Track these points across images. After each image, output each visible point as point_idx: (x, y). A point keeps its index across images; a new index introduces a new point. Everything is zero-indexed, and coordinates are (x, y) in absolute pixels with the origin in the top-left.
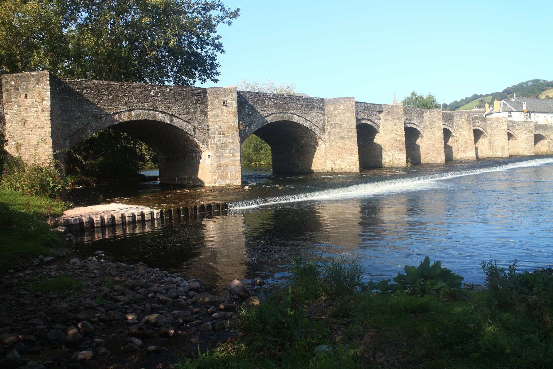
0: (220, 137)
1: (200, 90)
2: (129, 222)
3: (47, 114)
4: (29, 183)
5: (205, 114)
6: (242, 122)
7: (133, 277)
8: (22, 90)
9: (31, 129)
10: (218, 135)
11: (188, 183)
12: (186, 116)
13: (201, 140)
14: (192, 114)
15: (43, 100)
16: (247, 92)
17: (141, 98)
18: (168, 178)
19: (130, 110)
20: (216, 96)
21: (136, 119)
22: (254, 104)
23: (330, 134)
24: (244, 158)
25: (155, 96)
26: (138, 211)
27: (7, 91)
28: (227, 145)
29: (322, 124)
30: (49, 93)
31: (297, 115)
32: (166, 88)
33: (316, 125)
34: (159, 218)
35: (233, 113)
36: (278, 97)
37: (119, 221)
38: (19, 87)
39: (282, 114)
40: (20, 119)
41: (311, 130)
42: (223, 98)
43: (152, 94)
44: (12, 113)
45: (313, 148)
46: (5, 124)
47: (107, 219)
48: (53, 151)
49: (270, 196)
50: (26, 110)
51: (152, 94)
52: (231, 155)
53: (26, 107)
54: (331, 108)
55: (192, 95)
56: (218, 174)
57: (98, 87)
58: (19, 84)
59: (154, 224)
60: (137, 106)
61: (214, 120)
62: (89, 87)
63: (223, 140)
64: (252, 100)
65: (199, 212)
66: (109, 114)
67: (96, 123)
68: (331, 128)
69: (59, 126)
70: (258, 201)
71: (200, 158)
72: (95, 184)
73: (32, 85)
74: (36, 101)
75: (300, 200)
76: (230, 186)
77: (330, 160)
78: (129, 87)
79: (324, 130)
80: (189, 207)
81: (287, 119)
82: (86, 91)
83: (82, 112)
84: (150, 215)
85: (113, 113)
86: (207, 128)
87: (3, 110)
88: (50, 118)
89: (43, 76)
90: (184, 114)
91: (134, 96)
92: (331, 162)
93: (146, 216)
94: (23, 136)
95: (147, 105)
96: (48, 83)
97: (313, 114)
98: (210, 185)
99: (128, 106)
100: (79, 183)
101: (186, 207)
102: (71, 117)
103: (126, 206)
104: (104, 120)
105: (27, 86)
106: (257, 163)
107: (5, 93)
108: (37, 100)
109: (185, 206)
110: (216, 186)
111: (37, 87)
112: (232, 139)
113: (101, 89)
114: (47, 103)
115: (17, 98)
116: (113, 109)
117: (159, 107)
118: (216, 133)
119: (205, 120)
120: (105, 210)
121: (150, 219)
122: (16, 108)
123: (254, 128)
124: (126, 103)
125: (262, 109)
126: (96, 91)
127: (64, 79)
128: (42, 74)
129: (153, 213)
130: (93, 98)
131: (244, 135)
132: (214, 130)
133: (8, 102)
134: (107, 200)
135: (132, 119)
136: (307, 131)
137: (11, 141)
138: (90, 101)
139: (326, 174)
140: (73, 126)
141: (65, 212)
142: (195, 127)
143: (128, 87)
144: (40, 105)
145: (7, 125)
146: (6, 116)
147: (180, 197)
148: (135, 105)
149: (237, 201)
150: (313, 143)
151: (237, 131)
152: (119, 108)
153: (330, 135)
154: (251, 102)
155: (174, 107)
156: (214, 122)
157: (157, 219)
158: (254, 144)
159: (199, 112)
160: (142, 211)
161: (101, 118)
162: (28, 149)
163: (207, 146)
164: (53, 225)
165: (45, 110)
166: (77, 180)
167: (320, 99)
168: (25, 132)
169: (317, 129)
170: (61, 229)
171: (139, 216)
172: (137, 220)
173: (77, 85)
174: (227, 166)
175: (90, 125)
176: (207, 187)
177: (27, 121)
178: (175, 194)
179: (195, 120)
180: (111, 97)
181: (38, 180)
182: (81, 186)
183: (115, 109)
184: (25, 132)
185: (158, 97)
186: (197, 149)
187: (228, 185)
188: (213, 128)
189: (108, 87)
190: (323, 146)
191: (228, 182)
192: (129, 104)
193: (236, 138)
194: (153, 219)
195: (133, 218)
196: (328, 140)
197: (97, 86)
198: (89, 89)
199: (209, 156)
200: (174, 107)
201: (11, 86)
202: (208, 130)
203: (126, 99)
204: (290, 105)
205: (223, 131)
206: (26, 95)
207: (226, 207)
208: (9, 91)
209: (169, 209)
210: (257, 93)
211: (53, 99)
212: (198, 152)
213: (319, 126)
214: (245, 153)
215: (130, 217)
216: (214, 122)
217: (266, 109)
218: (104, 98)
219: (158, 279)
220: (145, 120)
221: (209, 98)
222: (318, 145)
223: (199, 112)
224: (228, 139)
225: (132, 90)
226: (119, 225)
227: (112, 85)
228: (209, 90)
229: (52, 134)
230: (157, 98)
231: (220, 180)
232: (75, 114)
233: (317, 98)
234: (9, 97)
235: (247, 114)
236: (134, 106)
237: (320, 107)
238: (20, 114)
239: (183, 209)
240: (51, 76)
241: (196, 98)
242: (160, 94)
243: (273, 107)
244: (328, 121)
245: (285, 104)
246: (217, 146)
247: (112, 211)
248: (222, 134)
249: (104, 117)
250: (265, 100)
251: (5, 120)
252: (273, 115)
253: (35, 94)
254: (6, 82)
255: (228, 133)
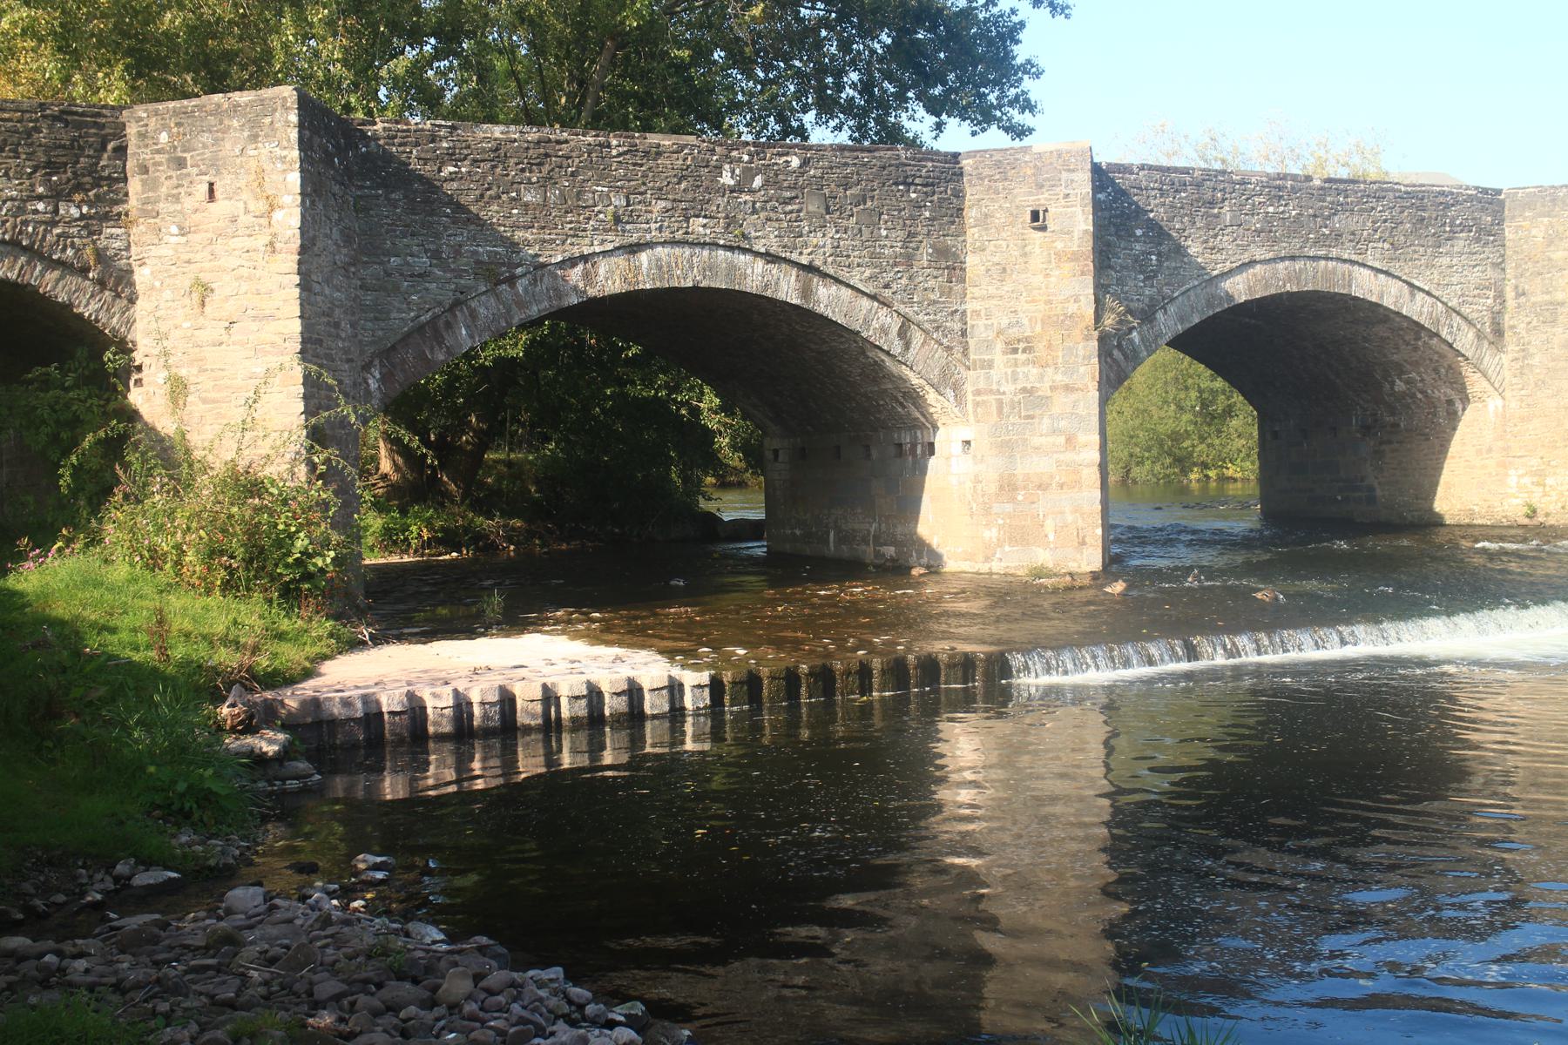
0: (1016, 365)
1: (933, 161)
2: (574, 720)
3: (288, 261)
4: (201, 538)
5: (950, 264)
6: (1116, 296)
7: (402, 1015)
8: (198, 166)
9: (227, 324)
10: (1004, 353)
11: (878, 554)
12: (867, 273)
13: (935, 375)
14: (895, 264)
15: (272, 208)
16: (1142, 167)
17: (677, 197)
18: (798, 532)
19: (633, 249)
20: (1000, 185)
21: (658, 285)
22: (1171, 220)
23: (1525, 352)
24: (1155, 452)
25: (737, 189)
26: (617, 676)
27: (144, 170)
28: (1042, 398)
29: (1490, 309)
30: (295, 178)
31: (1372, 268)
32: (787, 154)
33: (1458, 313)
34: (705, 708)
35: (1074, 257)
36: (1279, 187)
37: (534, 716)
38: (187, 155)
39: (1299, 265)
40: (187, 283)
41: (1437, 335)
42: (1031, 194)
43: (727, 179)
44: (160, 257)
45: (1442, 412)
46: (132, 301)
47: (482, 703)
48: (309, 412)
49: (1211, 630)
50: (209, 248)
51: (727, 179)
52: (1062, 440)
53: (209, 235)
54: (1534, 232)
55: (897, 184)
56: (1001, 522)
57: (502, 152)
58: (188, 141)
59: (683, 733)
60: (660, 229)
61: (992, 290)
62: (466, 152)
63: (1026, 376)
64: (1163, 204)
65: (881, 690)
66: (544, 266)
67: (492, 300)
68: (1534, 323)
69: (337, 311)
70: (1153, 650)
71: (930, 450)
72: (512, 547)
73: (235, 143)
74: (247, 211)
75: (1350, 652)
76: (1049, 576)
77: (1521, 472)
78: (632, 150)
79: (1498, 332)
80: (838, 666)
81: (1322, 286)
82: (452, 169)
83: (436, 254)
84: (664, 692)
85: (560, 258)
86: (957, 326)
87: (128, 248)
88: (297, 279)
89: (275, 110)
90: (858, 265)
91: (652, 189)
92: (1527, 480)
93: (647, 696)
94: (197, 350)
95: (704, 226)
96: (294, 134)
97: (1445, 261)
98: (966, 566)
99: (624, 231)
100: (449, 539)
101: (824, 666)
102: (389, 275)
103: (579, 648)
104: (526, 290)
105: (215, 148)
106: (1212, 473)
107: (138, 177)
108: (252, 207)
109: (819, 662)
110: (991, 574)
111: (252, 153)
112: (1065, 373)
113: (512, 161)
114: (289, 219)
115: (177, 198)
116: (563, 243)
117: (753, 234)
118: (1000, 346)
119: (951, 289)
120: (481, 662)
121: (666, 708)
122: (174, 240)
123: (1169, 323)
124: (617, 220)
125: (1206, 241)
126: (494, 167)
127: (364, 123)
128: (271, 99)
129: (681, 685)
130: (482, 196)
131: (1126, 356)
132: (991, 335)
133: (146, 214)
134: (514, 622)
135: (641, 287)
136: (1419, 338)
137: (153, 368)
138: (471, 212)
139: (1495, 532)
140: (400, 311)
141: (328, 667)
142: (907, 321)
143: (625, 153)
144: (260, 225)
145: (141, 307)
146: (136, 269)
147: (823, 616)
148: (653, 226)
149: (1059, 644)
150: (1443, 392)
151: (1087, 338)
152: (587, 241)
153: (1524, 357)
154: (1158, 213)
155: (820, 234)
156: (991, 297)
157: (697, 713)
158: (1201, 391)
159: (925, 255)
160: (631, 674)
161: (512, 280)
162: (214, 401)
163: (959, 399)
164: (240, 723)
165: (278, 245)
166: (442, 529)
167: (1485, 191)
168: (202, 336)
169: (1464, 326)
170: (268, 743)
171: (618, 694)
172: (607, 713)
173: (417, 144)
174: (1039, 487)
175: (469, 307)
176: (953, 574)
177: (212, 290)
178: (806, 602)
179: (909, 292)
180: (553, 195)
181: (238, 528)
182: (454, 554)
183: (572, 244)
184: (202, 336)
185: (752, 191)
186: (918, 415)
187: (1039, 573)
188: (986, 326)
189: (543, 154)
190: (1491, 408)
191: (1044, 557)
192: (628, 223)
193: (1082, 369)
194: (676, 714)
195: (590, 705)
196: (1515, 381)
197: (497, 149)
198: (466, 163)
199: (968, 443)
200: (820, 234)
201: (158, 152)
202: (964, 333)
203: (618, 201)
204: (1338, 222)
205: (1027, 339)
206: (211, 185)
207: (1006, 671)
208: (151, 169)
209: (750, 672)
210: (1186, 171)
211: (313, 203)
212: (922, 427)
213: (1475, 315)
214: (1161, 429)
215: (577, 698)
216: (991, 297)
217: (1225, 240)
218: (528, 198)
219: (516, 1032)
220: (695, 289)
221: (972, 193)
222: (1466, 400)
223: (925, 255)
224: (1050, 371)
225: (641, 165)
226: (528, 730)
227: (559, 142)
228: (970, 161)
229: (303, 343)
230: (745, 197)
231: (1007, 548)
232: (408, 264)
233: (1468, 188)
234: (150, 194)
235: (1140, 264)
236: (649, 231)
237: (1479, 230)
238: (189, 262)
239: (811, 674)
240: (305, 104)
241: (913, 196)
242: (758, 181)
243: (1259, 232)
244: (1520, 294)
245: (1315, 216)
246: (1000, 404)
247: (507, 668)
248: (1024, 351)
249: (524, 275)
250: (1224, 200)
251: (132, 284)
252: (1258, 267)
253: (242, 183)
254: (142, 136)
255: (1049, 346)
